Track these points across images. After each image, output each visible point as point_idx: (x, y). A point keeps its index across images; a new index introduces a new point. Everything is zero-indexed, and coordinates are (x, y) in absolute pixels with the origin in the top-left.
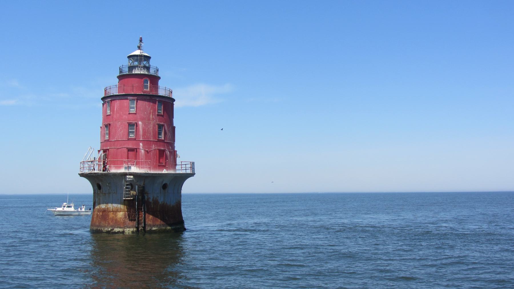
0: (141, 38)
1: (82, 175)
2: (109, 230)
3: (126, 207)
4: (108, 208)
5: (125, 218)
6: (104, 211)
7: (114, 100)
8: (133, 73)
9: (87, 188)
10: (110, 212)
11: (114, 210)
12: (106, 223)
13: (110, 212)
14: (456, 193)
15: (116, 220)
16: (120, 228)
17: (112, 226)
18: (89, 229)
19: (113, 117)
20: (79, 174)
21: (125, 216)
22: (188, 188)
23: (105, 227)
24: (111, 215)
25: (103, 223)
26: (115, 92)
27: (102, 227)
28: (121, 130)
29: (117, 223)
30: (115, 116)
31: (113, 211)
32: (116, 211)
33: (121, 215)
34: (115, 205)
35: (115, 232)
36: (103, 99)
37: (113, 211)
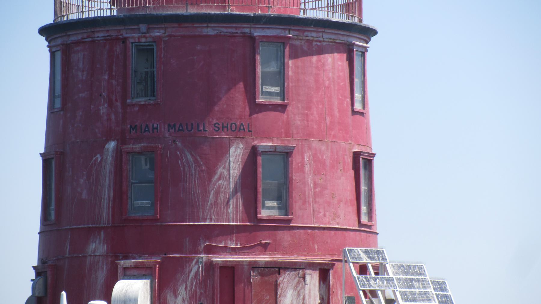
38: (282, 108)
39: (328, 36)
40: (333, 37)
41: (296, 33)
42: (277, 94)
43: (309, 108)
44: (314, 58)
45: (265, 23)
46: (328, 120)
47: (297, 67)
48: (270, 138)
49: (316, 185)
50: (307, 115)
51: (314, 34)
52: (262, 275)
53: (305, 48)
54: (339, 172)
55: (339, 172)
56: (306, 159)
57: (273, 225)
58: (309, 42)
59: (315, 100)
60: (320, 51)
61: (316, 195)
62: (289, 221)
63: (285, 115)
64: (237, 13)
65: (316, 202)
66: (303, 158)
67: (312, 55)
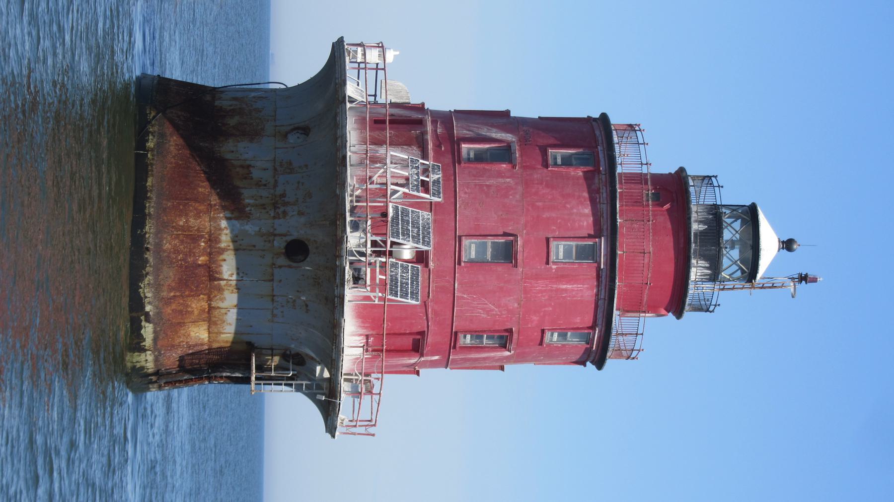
0: (814, 280)
1: (338, 49)
2: (148, 308)
3: (229, 345)
4: (220, 290)
5: (189, 347)
6: (212, 274)
7: (598, 277)
8: (694, 261)
9: (293, 64)
10: (210, 299)
11: (216, 313)
12: (171, 289)
13: (210, 299)
14: (269, 20)
15: (181, 324)
16: (155, 340)
17: (159, 314)
18: (149, 72)
19: (537, 277)
20: (342, 37)
21: (196, 345)
22: (287, 408)
23: (157, 287)
24: (197, 305)
25: (170, 275)
26: (627, 162)
27: (157, 271)
28: (488, 312)
29: (169, 327)
30: (540, 285)
31: (211, 308)
32: (210, 317)
33: (199, 334)
34: (232, 316)
35: (140, 328)
36: (604, 117)
37: (211, 308)
38: (546, 166)
39: (605, 208)
40: (605, 215)
41: (604, 179)
42: (557, 258)
43: (547, 186)
44: (586, 195)
45: (608, 155)
46: (540, 204)
47: (578, 178)
48: (521, 156)
49: (489, 186)
50: (542, 184)
51: (605, 195)
52: (417, 138)
53: (593, 187)
54: (500, 213)
55: (500, 213)
56: (508, 180)
57: (456, 158)
58: (598, 191)
59: (554, 192)
60: (593, 202)
61: (481, 186)
62: (459, 163)
63: (540, 167)
64: (617, 286)
65: (476, 185)
66: (508, 177)
67: (589, 193)
